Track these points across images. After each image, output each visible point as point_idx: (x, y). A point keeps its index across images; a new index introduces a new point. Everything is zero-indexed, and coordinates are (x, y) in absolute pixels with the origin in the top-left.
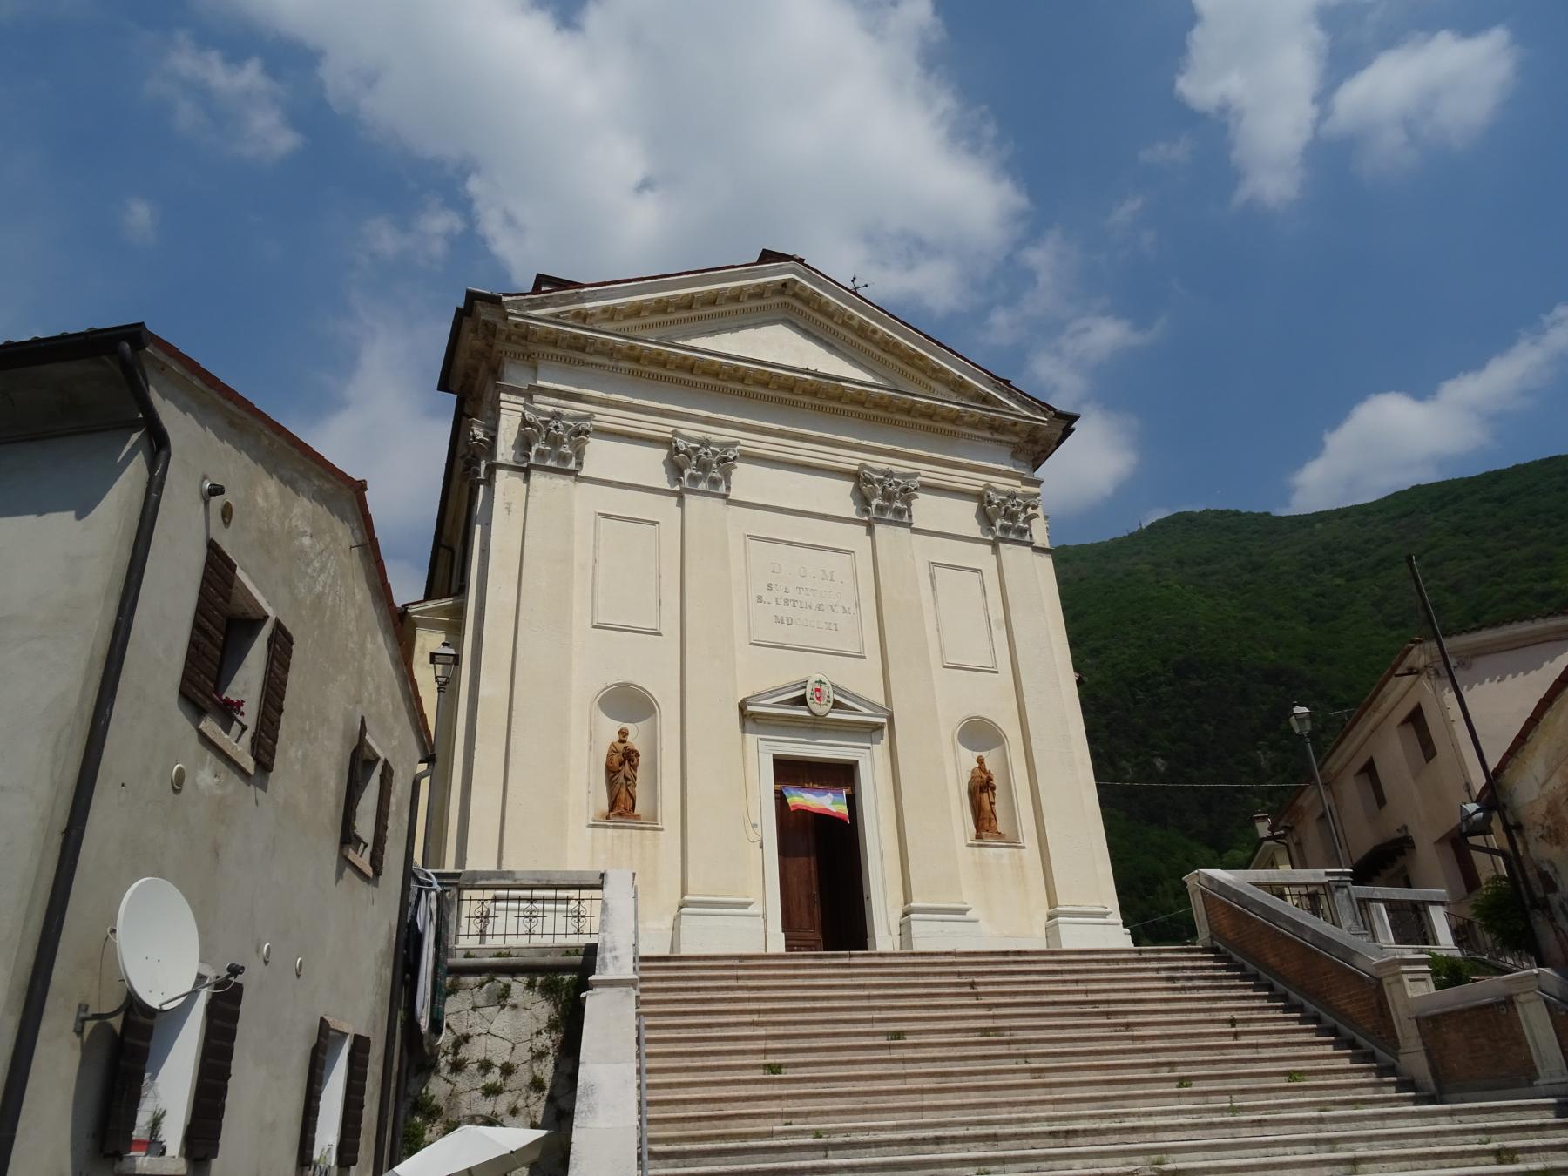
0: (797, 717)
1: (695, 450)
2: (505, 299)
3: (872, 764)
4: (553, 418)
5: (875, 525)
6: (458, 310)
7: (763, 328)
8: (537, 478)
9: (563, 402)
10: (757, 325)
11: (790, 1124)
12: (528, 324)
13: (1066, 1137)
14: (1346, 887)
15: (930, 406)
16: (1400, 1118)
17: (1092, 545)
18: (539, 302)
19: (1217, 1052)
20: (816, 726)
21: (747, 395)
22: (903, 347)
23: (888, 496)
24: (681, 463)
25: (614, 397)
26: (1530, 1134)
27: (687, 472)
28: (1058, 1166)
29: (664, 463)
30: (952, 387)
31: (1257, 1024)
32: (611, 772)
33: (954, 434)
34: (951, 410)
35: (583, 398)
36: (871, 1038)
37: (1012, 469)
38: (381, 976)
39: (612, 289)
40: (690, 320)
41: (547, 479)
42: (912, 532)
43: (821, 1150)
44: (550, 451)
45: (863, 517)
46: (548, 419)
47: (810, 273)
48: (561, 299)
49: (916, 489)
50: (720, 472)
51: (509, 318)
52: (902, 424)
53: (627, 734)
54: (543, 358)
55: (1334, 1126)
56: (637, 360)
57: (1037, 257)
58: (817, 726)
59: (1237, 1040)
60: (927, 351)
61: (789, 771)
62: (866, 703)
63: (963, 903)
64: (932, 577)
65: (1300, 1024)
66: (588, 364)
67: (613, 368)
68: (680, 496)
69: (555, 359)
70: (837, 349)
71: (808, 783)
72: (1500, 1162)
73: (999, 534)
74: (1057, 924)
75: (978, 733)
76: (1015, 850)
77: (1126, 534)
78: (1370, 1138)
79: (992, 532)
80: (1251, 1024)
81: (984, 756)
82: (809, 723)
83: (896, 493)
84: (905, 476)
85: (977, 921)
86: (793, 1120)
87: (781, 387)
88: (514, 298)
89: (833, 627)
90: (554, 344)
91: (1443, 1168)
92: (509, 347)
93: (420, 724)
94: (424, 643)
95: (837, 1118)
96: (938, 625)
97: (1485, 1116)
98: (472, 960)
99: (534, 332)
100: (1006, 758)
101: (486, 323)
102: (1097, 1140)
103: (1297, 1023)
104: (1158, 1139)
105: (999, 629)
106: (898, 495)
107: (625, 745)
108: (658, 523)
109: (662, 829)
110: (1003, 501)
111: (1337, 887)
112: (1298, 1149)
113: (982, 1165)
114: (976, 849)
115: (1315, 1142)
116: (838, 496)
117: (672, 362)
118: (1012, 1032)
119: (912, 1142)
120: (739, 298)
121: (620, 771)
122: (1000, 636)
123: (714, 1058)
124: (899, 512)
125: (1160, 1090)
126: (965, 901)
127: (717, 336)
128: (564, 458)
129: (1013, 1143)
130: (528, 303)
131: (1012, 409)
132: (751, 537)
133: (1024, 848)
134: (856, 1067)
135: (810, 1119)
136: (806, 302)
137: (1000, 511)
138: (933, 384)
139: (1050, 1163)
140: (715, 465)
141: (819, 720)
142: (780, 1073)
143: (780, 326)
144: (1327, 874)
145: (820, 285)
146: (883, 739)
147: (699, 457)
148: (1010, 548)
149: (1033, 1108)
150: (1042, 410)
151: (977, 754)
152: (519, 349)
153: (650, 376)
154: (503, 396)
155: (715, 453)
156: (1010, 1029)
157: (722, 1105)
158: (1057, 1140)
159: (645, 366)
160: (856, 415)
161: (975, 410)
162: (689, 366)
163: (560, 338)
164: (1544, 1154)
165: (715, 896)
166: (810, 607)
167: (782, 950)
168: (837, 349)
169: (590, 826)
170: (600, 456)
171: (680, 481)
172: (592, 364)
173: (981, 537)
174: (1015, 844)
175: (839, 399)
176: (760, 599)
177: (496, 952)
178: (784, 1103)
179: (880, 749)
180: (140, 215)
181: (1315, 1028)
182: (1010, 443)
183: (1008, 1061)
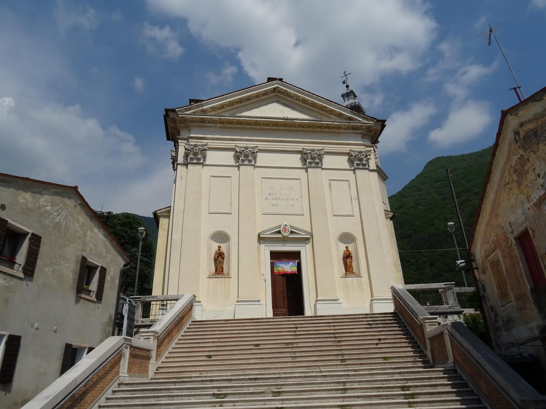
0: (278, 238)
1: (243, 151)
2: (177, 110)
3: (305, 251)
4: (195, 146)
5: (308, 169)
7: (268, 105)
8: (190, 167)
9: (199, 141)
10: (266, 104)
11: (202, 374)
12: (185, 116)
13: (255, 380)
14: (452, 289)
16: (379, 375)
17: (474, 153)
19: (365, 350)
20: (285, 240)
21: (262, 129)
23: (313, 158)
24: (239, 156)
25: (216, 136)
26: (424, 381)
27: (355, 162)
28: (245, 389)
31: (389, 340)
32: (216, 260)
33: (339, 133)
34: (336, 125)
35: (205, 138)
36: (248, 346)
37: (361, 142)
38: (105, 330)
39: (212, 101)
40: (242, 106)
41: (194, 167)
42: (369, 171)
43: (174, 383)
44: (194, 157)
45: (304, 166)
46: (193, 147)
47: (283, 83)
49: (323, 154)
50: (252, 157)
51: (179, 116)
52: (319, 132)
53: (220, 247)
55: (353, 377)
56: (223, 123)
57: (444, 47)
58: (285, 240)
59: (377, 346)
60: (327, 105)
61: (276, 256)
62: (302, 231)
64: (330, 185)
65: (406, 340)
66: (207, 127)
67: (215, 127)
68: (354, 171)
69: (196, 126)
70: (295, 108)
71: (284, 259)
72: (403, 390)
73: (355, 167)
74: (372, 303)
75: (346, 238)
76: (359, 278)
77: (488, 147)
78: (360, 382)
79: (354, 166)
80: (387, 340)
81: (348, 246)
83: (316, 157)
84: (319, 150)
86: (203, 373)
87: (273, 125)
88: (180, 109)
89: (292, 205)
90: (195, 122)
91: (380, 392)
92: (181, 125)
93: (122, 253)
94: (162, 223)
95: (217, 372)
96: (331, 201)
97: (414, 374)
98: (143, 323)
99: (188, 119)
100: (356, 246)
101: (172, 118)
102: (265, 381)
103: (405, 339)
104: (287, 381)
105: (355, 201)
106: (317, 157)
107: (219, 251)
108: (231, 177)
109: (231, 278)
110: (357, 154)
111: (448, 289)
112: (331, 385)
113: (219, 388)
114: (344, 278)
115: (339, 383)
116: (295, 160)
117: (234, 122)
118: (297, 344)
119: (203, 381)
120: (258, 96)
121: (217, 260)
122: (355, 203)
123: (194, 353)
124: (317, 163)
125: (329, 364)
126: (338, 297)
127: (252, 110)
128: (199, 159)
129: (237, 382)
131: (360, 121)
134: (236, 356)
135: (208, 372)
136: (283, 93)
137: (356, 158)
138: (331, 116)
139: (242, 388)
140: (250, 155)
142: (211, 358)
143: (275, 104)
144: (445, 285)
145: (287, 87)
147: (244, 153)
148: (360, 171)
149: (284, 369)
150: (372, 120)
152: (184, 125)
153: (228, 128)
154: (180, 141)
155: (250, 151)
156: (296, 343)
157: (185, 368)
158: (252, 381)
159: (226, 124)
160: (302, 131)
161: (345, 123)
162: (240, 123)
163: (196, 120)
164: (422, 388)
165: (247, 298)
167: (272, 316)
168: (295, 108)
169: (207, 278)
170: (212, 157)
171: (239, 162)
172: (208, 126)
173: (349, 168)
174: (359, 276)
175: (294, 126)
176: (266, 199)
177: (151, 320)
178: (204, 367)
179: (309, 246)
180: (139, 83)
181: (408, 342)
182: (361, 133)
183: (288, 354)
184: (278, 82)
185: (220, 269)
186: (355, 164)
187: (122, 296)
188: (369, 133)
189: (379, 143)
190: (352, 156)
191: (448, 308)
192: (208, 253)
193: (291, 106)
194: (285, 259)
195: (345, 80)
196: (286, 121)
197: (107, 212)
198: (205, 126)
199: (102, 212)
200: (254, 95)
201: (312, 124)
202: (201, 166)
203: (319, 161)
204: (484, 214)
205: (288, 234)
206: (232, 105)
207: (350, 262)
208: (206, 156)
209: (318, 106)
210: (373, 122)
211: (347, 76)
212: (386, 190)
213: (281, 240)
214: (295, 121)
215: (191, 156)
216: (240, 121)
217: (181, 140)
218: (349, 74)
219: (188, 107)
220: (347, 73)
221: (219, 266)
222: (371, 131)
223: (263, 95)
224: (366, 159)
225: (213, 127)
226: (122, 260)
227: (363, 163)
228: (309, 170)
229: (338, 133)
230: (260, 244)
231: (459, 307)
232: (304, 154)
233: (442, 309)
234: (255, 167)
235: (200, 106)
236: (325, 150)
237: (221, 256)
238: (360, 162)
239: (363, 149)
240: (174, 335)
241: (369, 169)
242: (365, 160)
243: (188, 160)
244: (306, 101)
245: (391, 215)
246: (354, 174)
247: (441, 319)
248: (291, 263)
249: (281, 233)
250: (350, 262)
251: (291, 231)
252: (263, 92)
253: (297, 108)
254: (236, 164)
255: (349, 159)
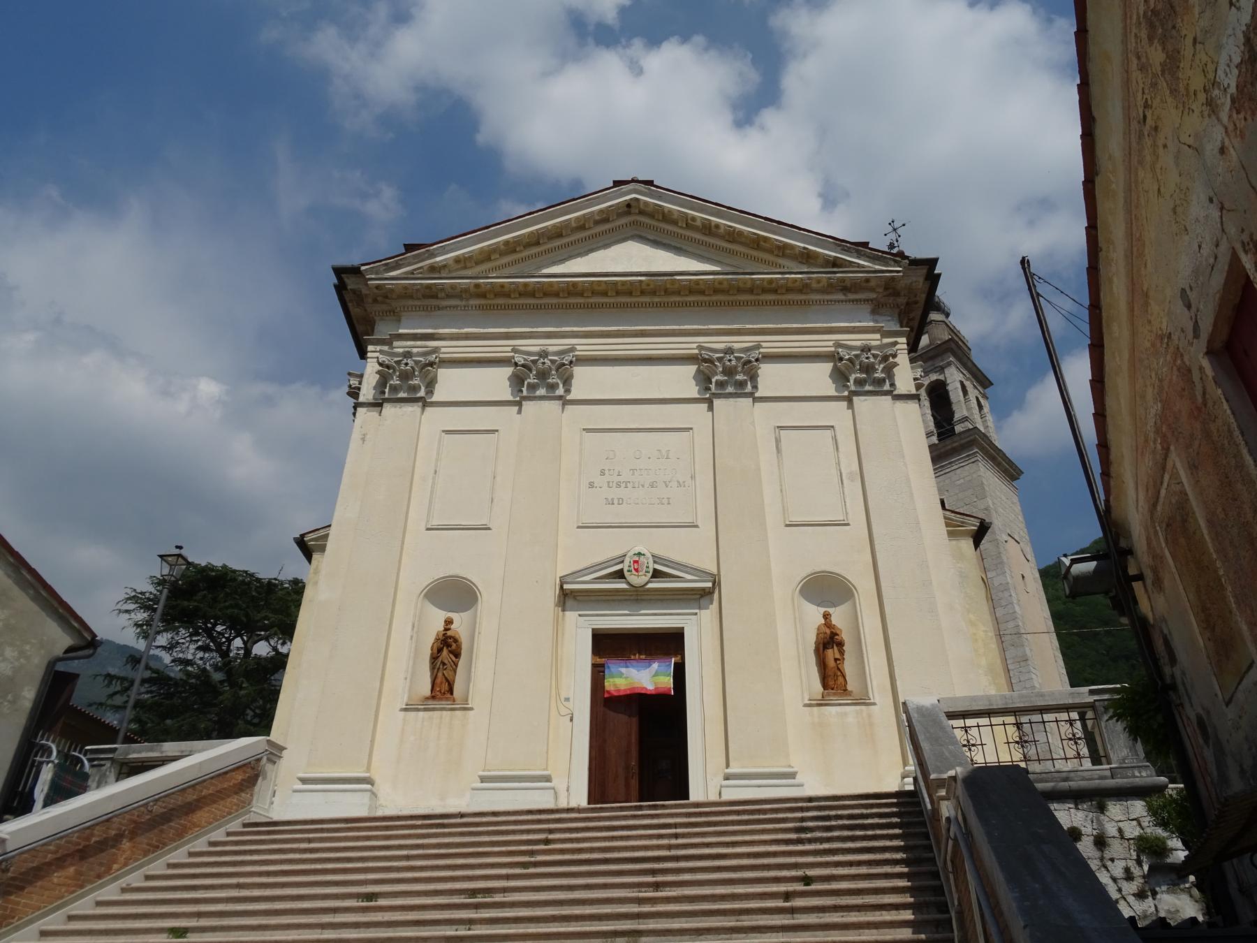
0: (617, 590)
1: (534, 362)
2: (363, 268)
6: (335, 286)
7: (612, 248)
8: (388, 409)
15: (771, 281)
18: (394, 264)
22: (745, 233)
27: (852, 378)
29: (509, 379)
30: (800, 260)
34: (795, 280)
35: (436, 336)
37: (871, 324)
42: (893, 400)
45: (706, 394)
48: (414, 259)
54: (404, 311)
58: (638, 597)
62: (689, 570)
63: (790, 766)
64: (778, 441)
67: (465, 307)
68: (849, 400)
71: (635, 655)
73: (853, 388)
76: (863, 707)
82: (631, 595)
83: (736, 367)
85: (802, 785)
89: (665, 501)
92: (377, 307)
99: (392, 290)
101: (354, 291)
106: (740, 369)
109: (471, 709)
110: (856, 356)
114: (815, 709)
116: (682, 380)
122: (853, 488)
124: (742, 384)
126: (792, 765)
128: (415, 389)
130: (384, 268)
131: (863, 266)
132: (587, 430)
133: (874, 704)
136: (651, 215)
138: (780, 261)
141: (641, 591)
142: (185, 937)
145: (660, 198)
146: (712, 604)
148: (866, 400)
150: (895, 261)
151: (822, 610)
152: (384, 307)
155: (553, 362)
159: (493, 299)
160: (699, 304)
165: (510, 770)
166: (643, 486)
170: (450, 383)
172: (446, 307)
174: (863, 700)
176: (591, 485)
179: (707, 616)
184: (637, 187)
185: (441, 683)
186: (852, 381)
187: (43, 742)
188: (891, 300)
189: (992, 387)
190: (841, 359)
191: (1108, 773)
192: (412, 637)
193: (673, 245)
194: (637, 655)
195: (894, 239)
196: (653, 278)
197: (290, 581)
198: (438, 307)
199: (278, 580)
200: (574, 225)
201: (725, 283)
202: (419, 406)
203: (745, 378)
204: (1115, 327)
205: (646, 579)
206: (514, 251)
207: (836, 660)
208: (437, 382)
209: (746, 237)
210: (900, 267)
211: (891, 229)
212: (1018, 503)
213: (627, 597)
214: (678, 278)
215: (395, 381)
216: (530, 288)
217: (373, 344)
218: (904, 225)
219: (393, 260)
220: (896, 225)
221: (440, 674)
222: (896, 294)
223: (597, 223)
224: (884, 367)
225: (459, 309)
226: (64, 631)
227: (875, 377)
228: (717, 402)
229: (803, 303)
230: (563, 610)
231: (1149, 772)
232: (704, 365)
233: (1084, 779)
234: (564, 405)
235: (427, 255)
236: (761, 350)
237: (449, 646)
238: (865, 376)
239: (874, 339)
240: (122, 860)
241: (895, 393)
242: (880, 369)
243: (384, 393)
244: (713, 229)
245: (975, 526)
246: (848, 409)
247: (1081, 814)
248: (655, 666)
249: (625, 578)
250: (836, 660)
251: (655, 570)
252: (598, 215)
253: (690, 249)
254: (514, 397)
255: (835, 369)
